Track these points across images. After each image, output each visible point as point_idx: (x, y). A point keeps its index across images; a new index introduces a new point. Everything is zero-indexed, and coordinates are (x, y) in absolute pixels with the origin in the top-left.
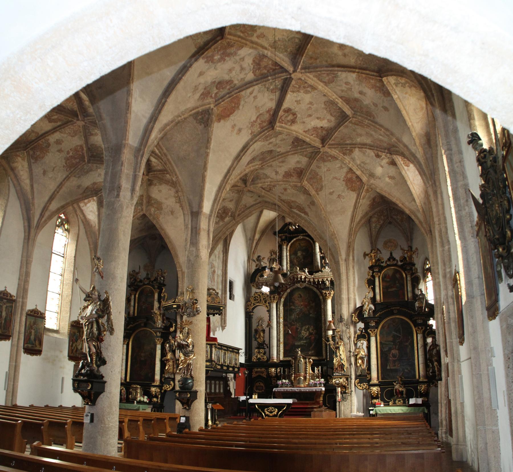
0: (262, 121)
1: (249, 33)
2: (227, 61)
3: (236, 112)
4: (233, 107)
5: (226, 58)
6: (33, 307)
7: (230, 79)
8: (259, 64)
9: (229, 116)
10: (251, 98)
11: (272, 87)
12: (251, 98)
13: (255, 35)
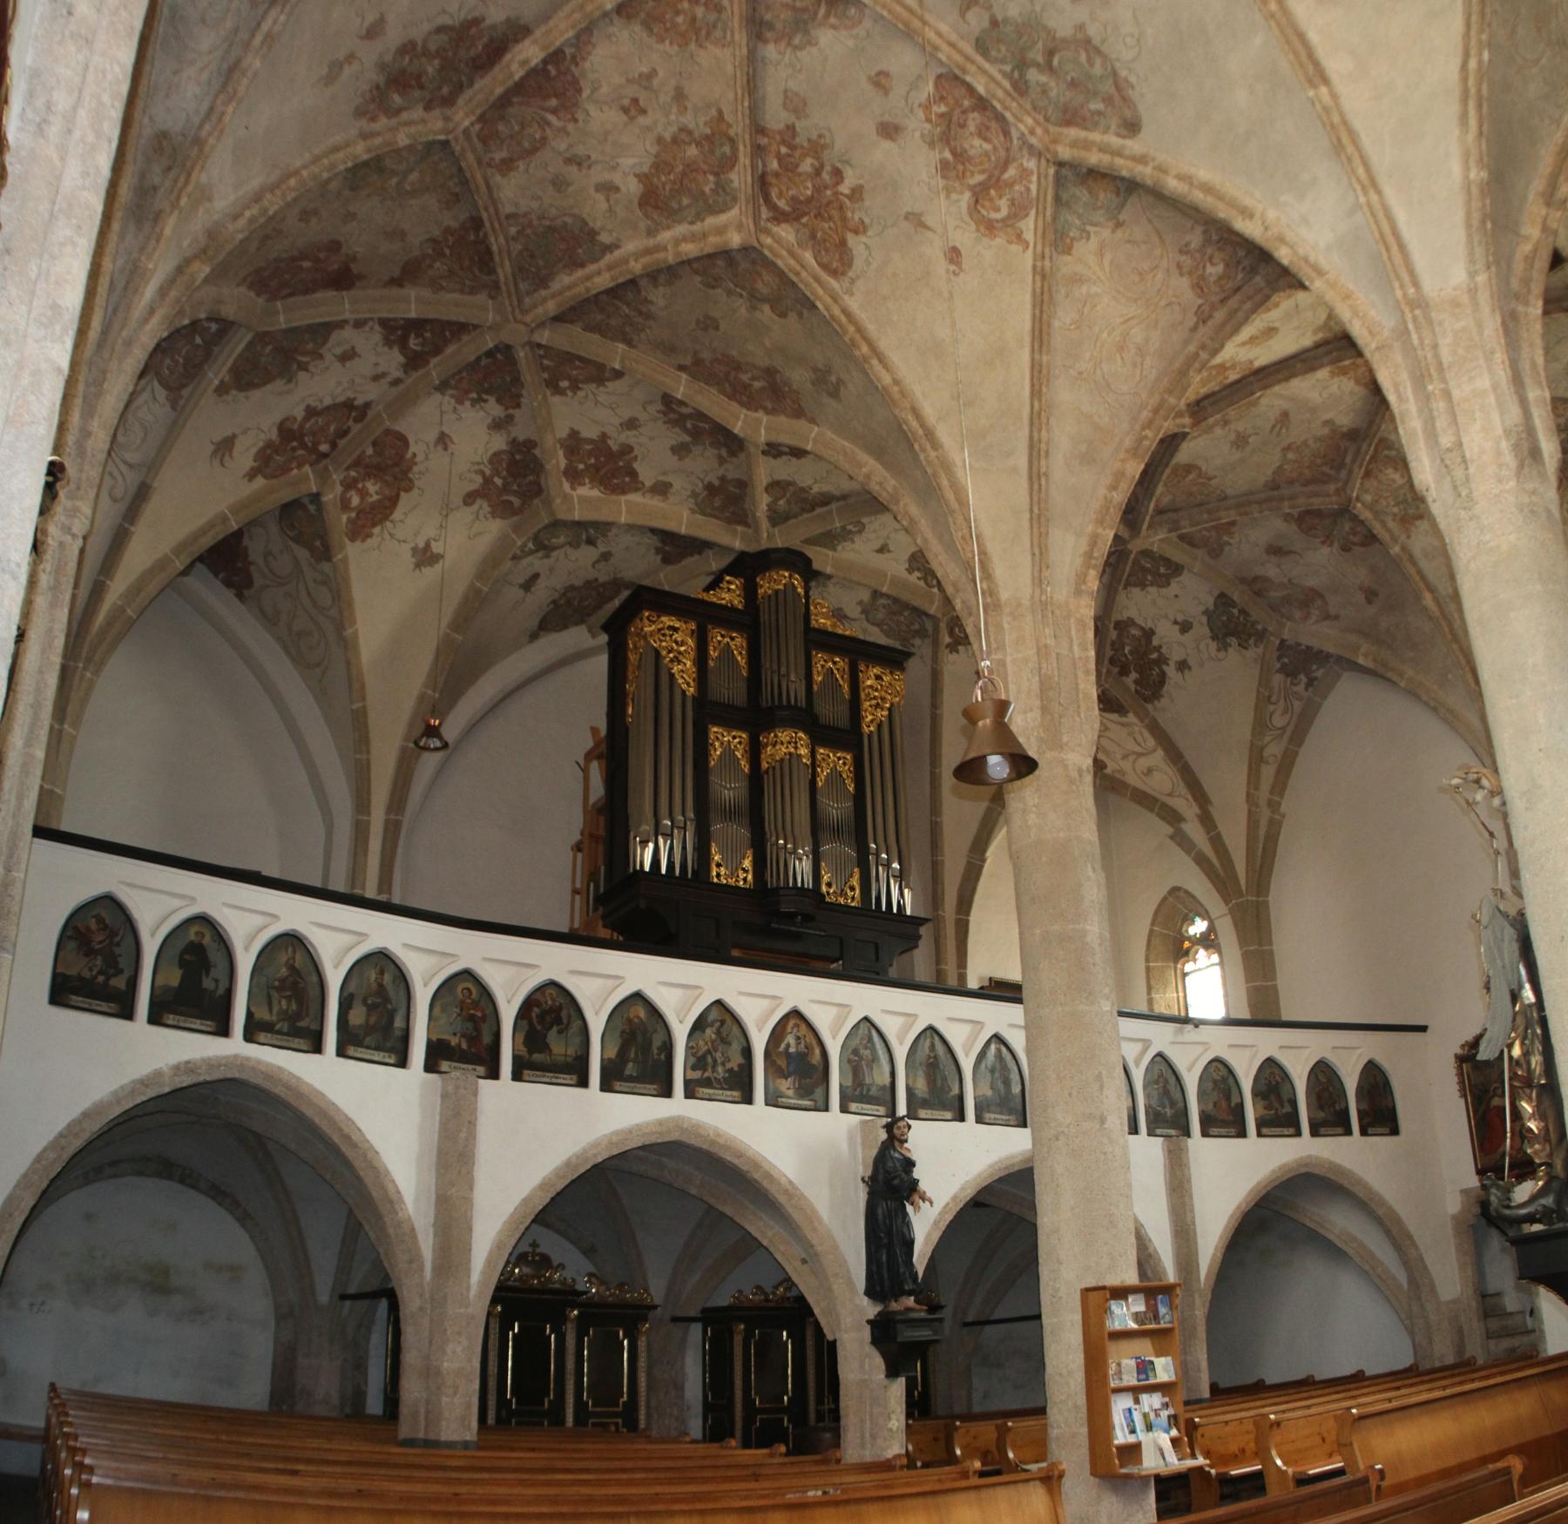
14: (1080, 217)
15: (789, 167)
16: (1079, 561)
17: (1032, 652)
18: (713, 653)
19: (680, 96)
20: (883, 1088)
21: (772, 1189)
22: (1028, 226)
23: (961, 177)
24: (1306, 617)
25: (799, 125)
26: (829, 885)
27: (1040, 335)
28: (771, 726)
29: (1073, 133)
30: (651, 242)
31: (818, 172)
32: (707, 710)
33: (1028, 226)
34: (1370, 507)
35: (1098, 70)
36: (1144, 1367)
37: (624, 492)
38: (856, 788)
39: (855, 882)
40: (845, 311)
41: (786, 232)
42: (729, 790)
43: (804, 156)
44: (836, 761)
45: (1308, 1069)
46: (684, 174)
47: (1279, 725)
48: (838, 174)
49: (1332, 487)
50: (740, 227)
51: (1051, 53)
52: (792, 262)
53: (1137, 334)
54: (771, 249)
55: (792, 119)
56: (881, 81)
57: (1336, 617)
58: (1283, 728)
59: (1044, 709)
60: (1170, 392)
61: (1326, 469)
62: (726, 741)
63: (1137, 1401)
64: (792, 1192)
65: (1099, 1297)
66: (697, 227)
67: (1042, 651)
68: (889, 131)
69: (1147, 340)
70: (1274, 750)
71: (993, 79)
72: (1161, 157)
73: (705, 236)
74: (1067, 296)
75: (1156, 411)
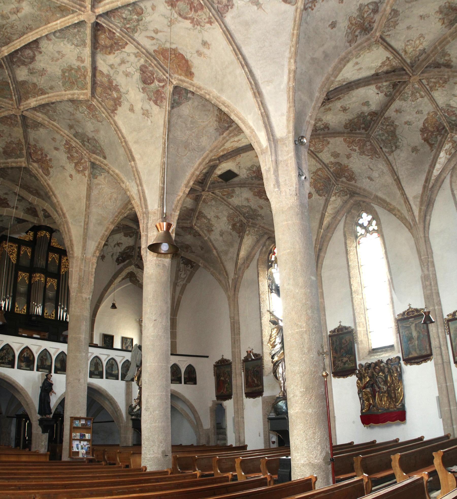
0: (191, 9)
1: (83, 71)
2: (117, 82)
3: (181, 52)
4: (176, 56)
5: (114, 84)
6: (336, 326)
7: (139, 71)
8: (111, 46)
9: (187, 61)
10: (159, 36)
11: (136, 17)
12: (159, 36)
13: (82, 65)
14: (99, 171)
15: (35, 152)
16: (95, 248)
17: (78, 269)
18: (22, 253)
19: (10, 135)
20: (49, 366)
21: (18, 388)
22: (87, 173)
23: (72, 160)
24: (187, 251)
25: (37, 145)
26: (46, 313)
27: (88, 197)
28: (35, 272)
29: (94, 156)
30: (6, 161)
31: (42, 154)
32: (18, 267)
33: (87, 173)
34: (199, 227)
35: (98, 145)
36: (83, 436)
37: (5, 208)
38: (57, 289)
39: (54, 313)
40: (48, 184)
41: (35, 165)
42: (22, 289)
43: (38, 151)
44: (52, 282)
45: (197, 371)
46: (12, 150)
47: (183, 277)
48: (46, 156)
49: (189, 221)
50: (25, 163)
51: (88, 140)
52: (36, 172)
53: (115, 196)
54: (31, 168)
55: (36, 143)
56: (54, 139)
57: (194, 253)
58: (184, 278)
59: (79, 283)
60: (123, 209)
61: (187, 217)
62: (23, 276)
63: (80, 443)
64: (22, 389)
65: (74, 419)
66: (16, 160)
67: (80, 270)
68: (56, 149)
69: (117, 197)
70: (181, 283)
71: (77, 143)
72: (110, 165)
73: (17, 162)
74: (96, 188)
75: (119, 213)
